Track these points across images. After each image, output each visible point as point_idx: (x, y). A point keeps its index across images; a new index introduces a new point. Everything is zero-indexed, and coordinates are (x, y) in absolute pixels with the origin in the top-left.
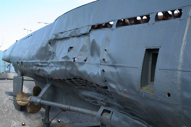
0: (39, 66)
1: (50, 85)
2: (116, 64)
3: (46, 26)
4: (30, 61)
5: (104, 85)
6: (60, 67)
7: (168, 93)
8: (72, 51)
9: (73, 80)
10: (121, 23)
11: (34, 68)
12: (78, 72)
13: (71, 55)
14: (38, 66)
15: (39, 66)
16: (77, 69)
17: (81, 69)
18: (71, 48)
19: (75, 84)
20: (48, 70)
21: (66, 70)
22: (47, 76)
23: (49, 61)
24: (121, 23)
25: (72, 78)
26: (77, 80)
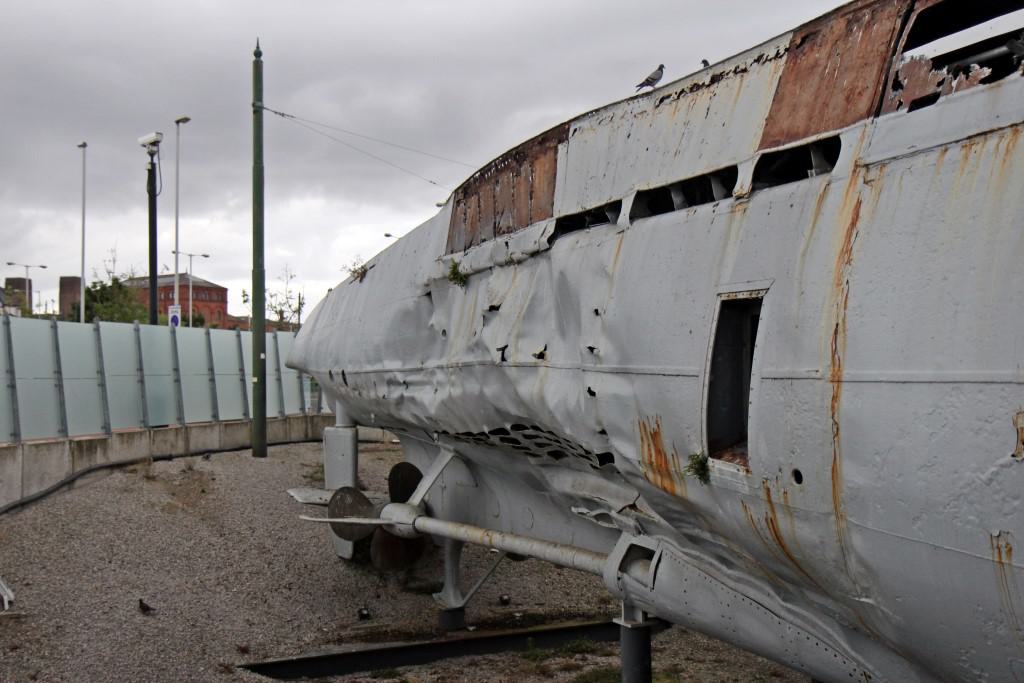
0: (398, 384)
1: (449, 456)
2: (630, 366)
3: (254, 304)
4: (369, 368)
5: (597, 448)
6: (463, 385)
7: (795, 467)
8: (496, 321)
9: (513, 435)
10: (653, 202)
11: (383, 391)
12: (520, 402)
13: (494, 335)
14: (391, 382)
15: (398, 384)
16: (515, 390)
17: (527, 388)
18: (494, 309)
19: (522, 448)
20: (429, 399)
21: (482, 394)
22: (426, 421)
23: (431, 364)
24: (653, 202)
25: (508, 427)
26: (527, 432)
